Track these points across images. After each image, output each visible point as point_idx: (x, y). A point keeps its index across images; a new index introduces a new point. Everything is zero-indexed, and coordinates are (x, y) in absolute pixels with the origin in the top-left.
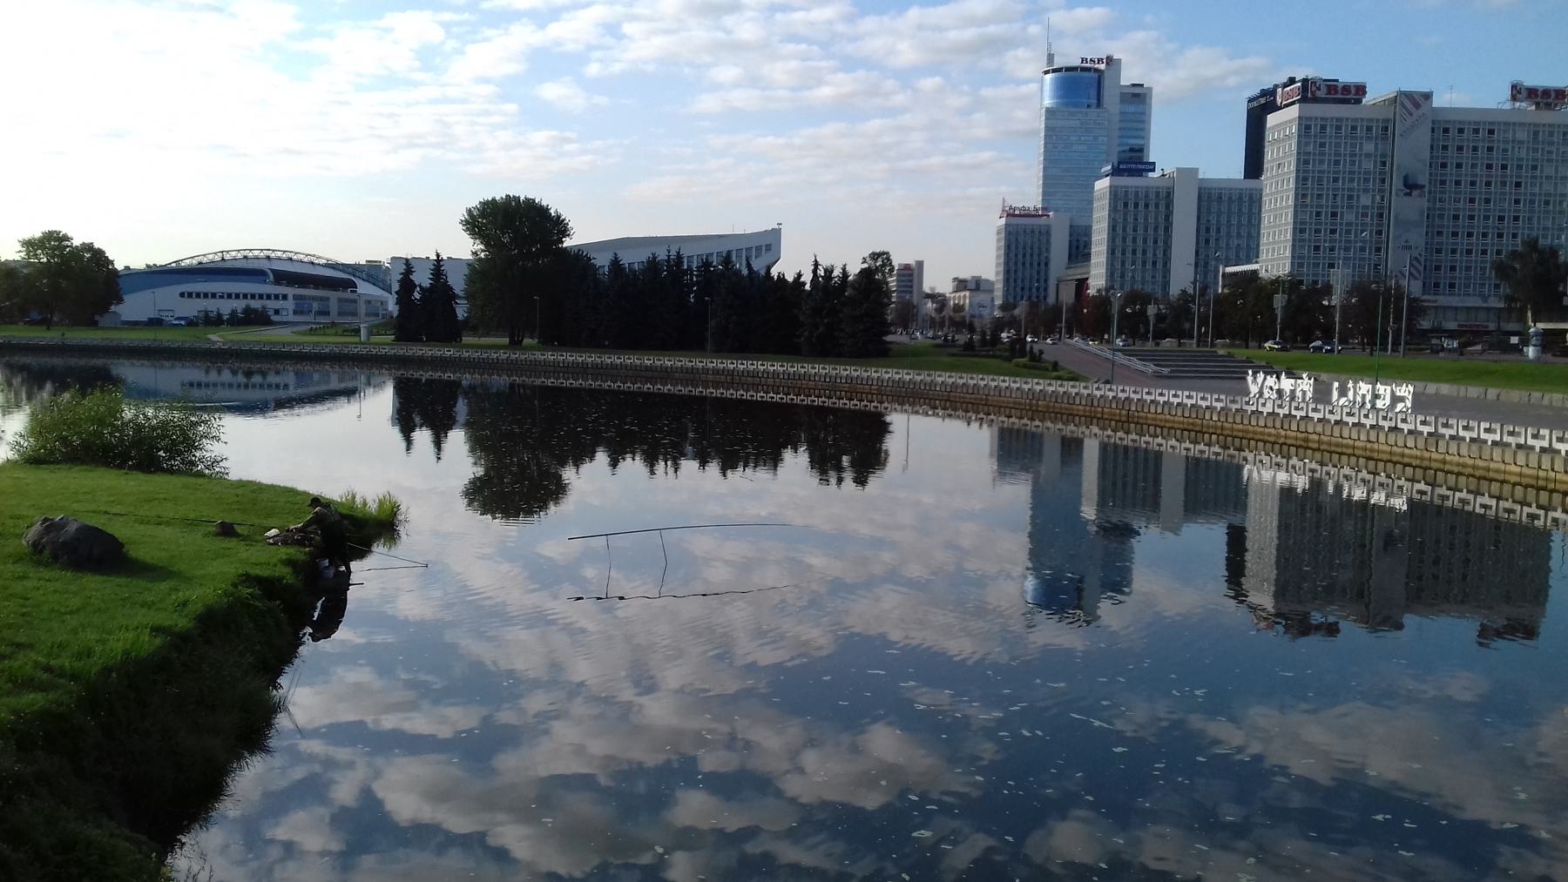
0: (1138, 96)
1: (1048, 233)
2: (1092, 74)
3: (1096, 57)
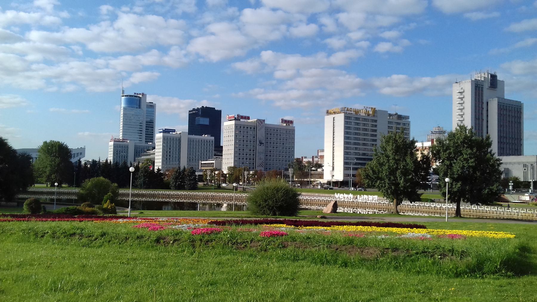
0: (151, 106)
1: (127, 147)
2: (137, 98)
3: (139, 93)
